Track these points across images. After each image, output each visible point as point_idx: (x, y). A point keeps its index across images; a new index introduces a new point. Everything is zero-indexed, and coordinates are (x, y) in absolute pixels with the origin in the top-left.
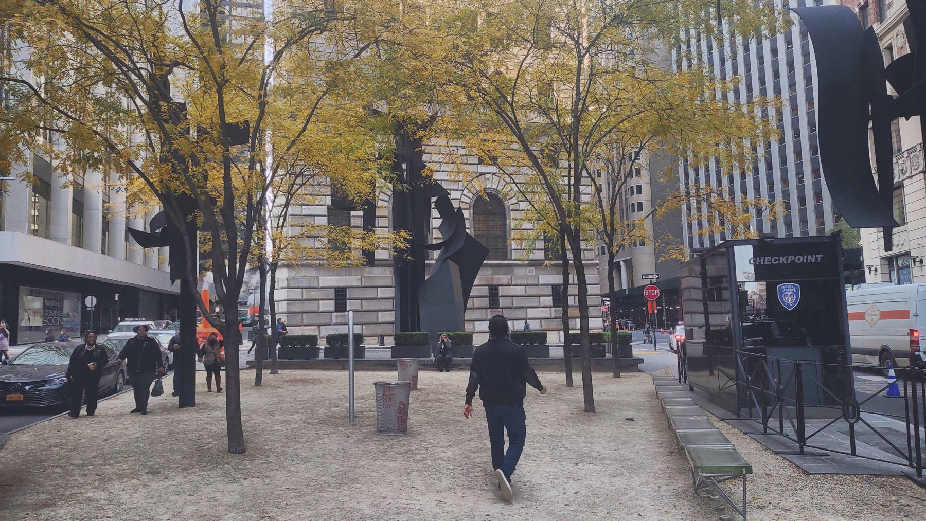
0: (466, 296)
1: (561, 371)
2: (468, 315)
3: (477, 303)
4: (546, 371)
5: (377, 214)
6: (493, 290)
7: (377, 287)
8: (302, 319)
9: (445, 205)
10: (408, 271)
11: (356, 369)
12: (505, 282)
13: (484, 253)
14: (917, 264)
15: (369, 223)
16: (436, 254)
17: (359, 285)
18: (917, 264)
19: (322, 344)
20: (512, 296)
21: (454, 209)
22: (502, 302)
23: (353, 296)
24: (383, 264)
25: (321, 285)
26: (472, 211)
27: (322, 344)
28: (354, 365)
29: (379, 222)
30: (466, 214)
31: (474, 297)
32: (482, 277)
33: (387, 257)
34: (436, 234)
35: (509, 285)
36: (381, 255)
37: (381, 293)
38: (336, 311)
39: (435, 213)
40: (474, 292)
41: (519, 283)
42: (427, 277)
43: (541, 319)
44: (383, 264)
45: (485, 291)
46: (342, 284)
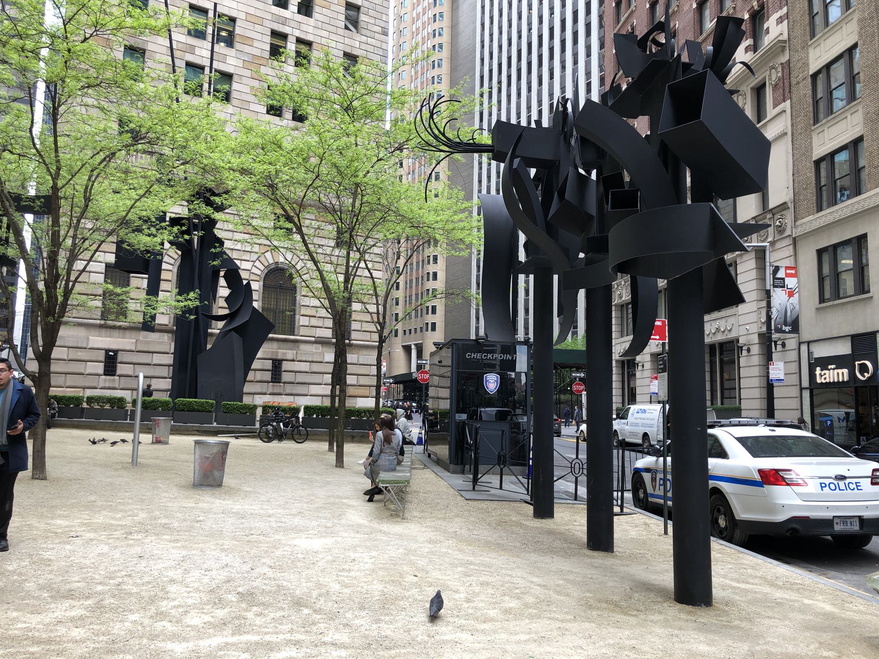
0: (247, 368)
1: (325, 441)
2: (247, 388)
3: (259, 376)
4: (812, 564)
5: (162, 277)
6: (277, 364)
7: (153, 353)
8: (65, 381)
9: (233, 276)
10: (189, 332)
11: (141, 432)
12: (290, 357)
13: (271, 328)
14: (779, 348)
15: (153, 289)
16: (221, 324)
17: (133, 349)
18: (779, 348)
19: (259, 412)
20: (296, 372)
21: (241, 279)
22: (286, 377)
23: (124, 360)
24: (163, 330)
25: (90, 346)
26: (262, 283)
27: (259, 412)
28: (140, 428)
29: (163, 286)
30: (255, 286)
31: (255, 370)
32: (266, 350)
33: (167, 323)
34: (222, 303)
35: (293, 360)
36: (162, 320)
37: (157, 359)
38: (105, 375)
39: (222, 282)
40: (256, 365)
41: (304, 359)
42: (209, 347)
43: (322, 396)
44: (163, 330)
45: (269, 364)
46: (114, 347)
